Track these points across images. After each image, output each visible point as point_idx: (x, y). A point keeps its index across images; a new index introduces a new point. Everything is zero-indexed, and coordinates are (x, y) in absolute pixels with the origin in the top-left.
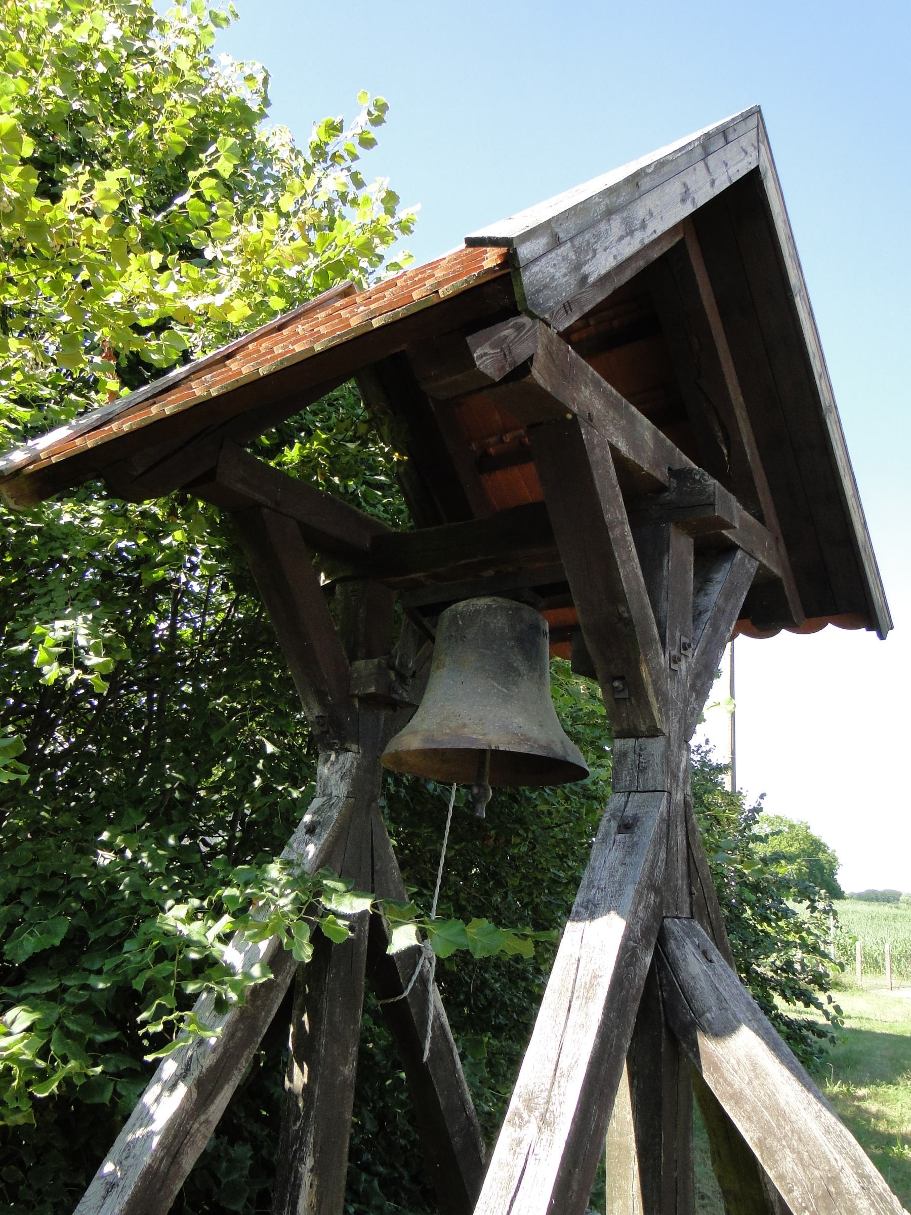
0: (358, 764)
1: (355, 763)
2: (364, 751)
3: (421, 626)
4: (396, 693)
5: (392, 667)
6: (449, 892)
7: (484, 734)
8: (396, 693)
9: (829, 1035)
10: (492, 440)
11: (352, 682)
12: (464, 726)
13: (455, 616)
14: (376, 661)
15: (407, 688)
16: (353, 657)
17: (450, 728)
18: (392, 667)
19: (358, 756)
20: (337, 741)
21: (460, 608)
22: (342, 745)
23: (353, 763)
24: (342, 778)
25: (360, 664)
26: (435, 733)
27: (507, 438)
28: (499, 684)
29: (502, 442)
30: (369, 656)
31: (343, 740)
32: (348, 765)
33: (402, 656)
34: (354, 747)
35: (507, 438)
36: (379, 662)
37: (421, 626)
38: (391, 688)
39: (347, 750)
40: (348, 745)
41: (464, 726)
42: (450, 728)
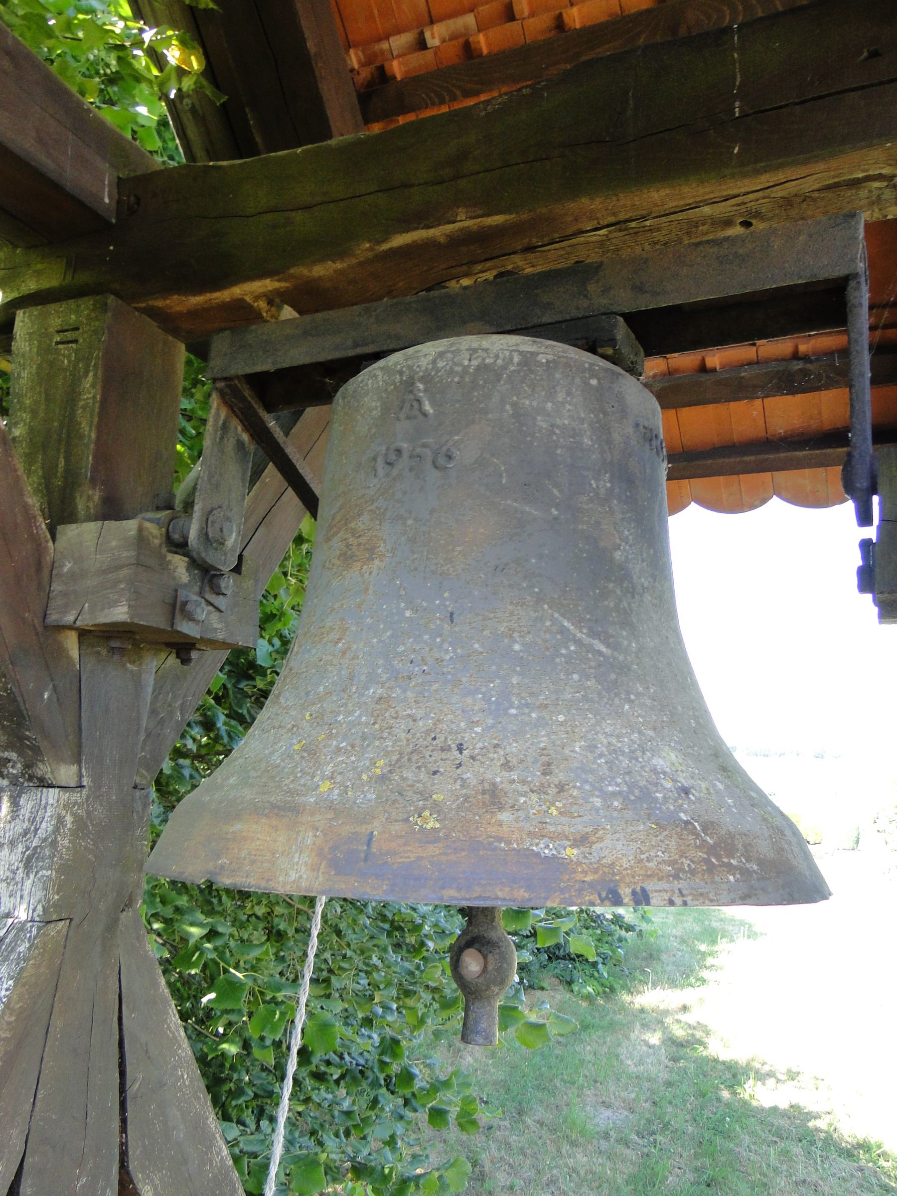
0: (78, 820)
1: (69, 819)
2: (97, 780)
3: (261, 434)
4: (190, 617)
5: (180, 546)
6: (256, 908)
7: (582, 841)
8: (190, 617)
9: (637, 929)
10: (399, 42)
11: (56, 587)
12: (494, 797)
13: (409, 385)
14: (130, 526)
15: (220, 601)
16: (61, 513)
17: (436, 808)
18: (180, 546)
19: (76, 796)
20: (14, 756)
21: (424, 362)
22: (28, 766)
23: (60, 820)
24: (28, 864)
25: (82, 535)
26: (376, 828)
27: (435, 36)
28: (579, 622)
29: (421, 44)
30: (112, 510)
31: (32, 755)
32: (46, 827)
33: (208, 515)
34: (66, 773)
35: (435, 36)
36: (140, 529)
37: (261, 434)
38: (176, 607)
39: (44, 784)
40: (42, 769)
41: (494, 797)
42: (436, 808)
